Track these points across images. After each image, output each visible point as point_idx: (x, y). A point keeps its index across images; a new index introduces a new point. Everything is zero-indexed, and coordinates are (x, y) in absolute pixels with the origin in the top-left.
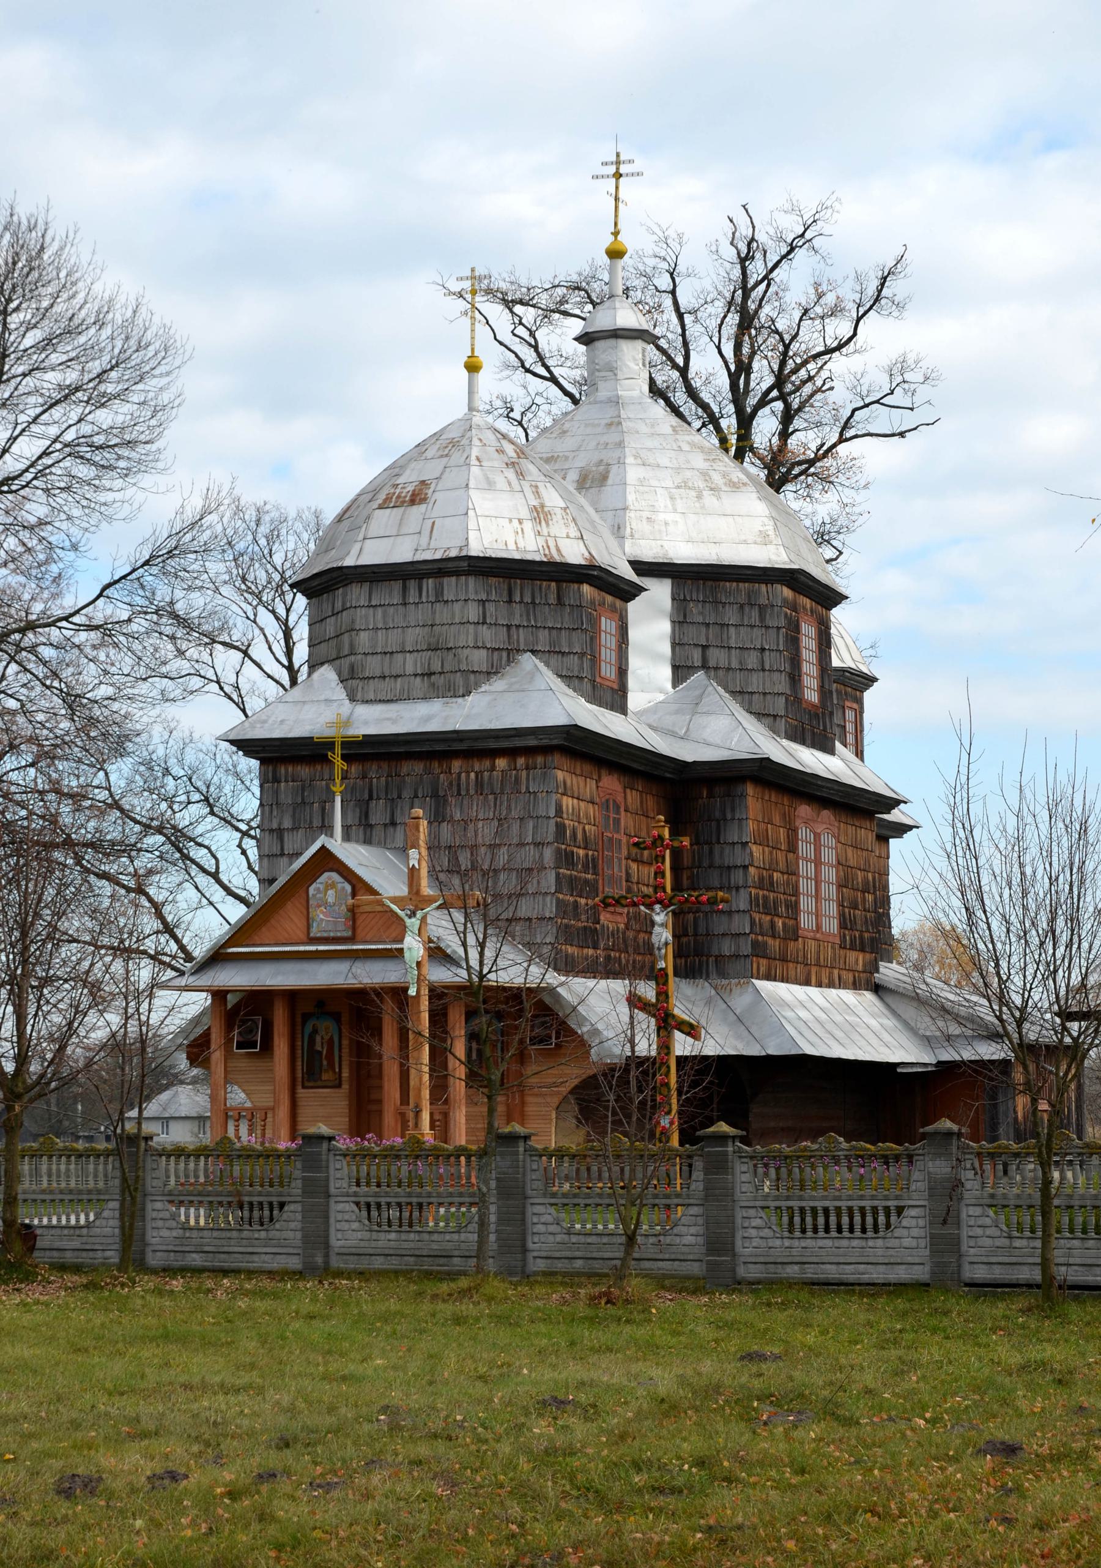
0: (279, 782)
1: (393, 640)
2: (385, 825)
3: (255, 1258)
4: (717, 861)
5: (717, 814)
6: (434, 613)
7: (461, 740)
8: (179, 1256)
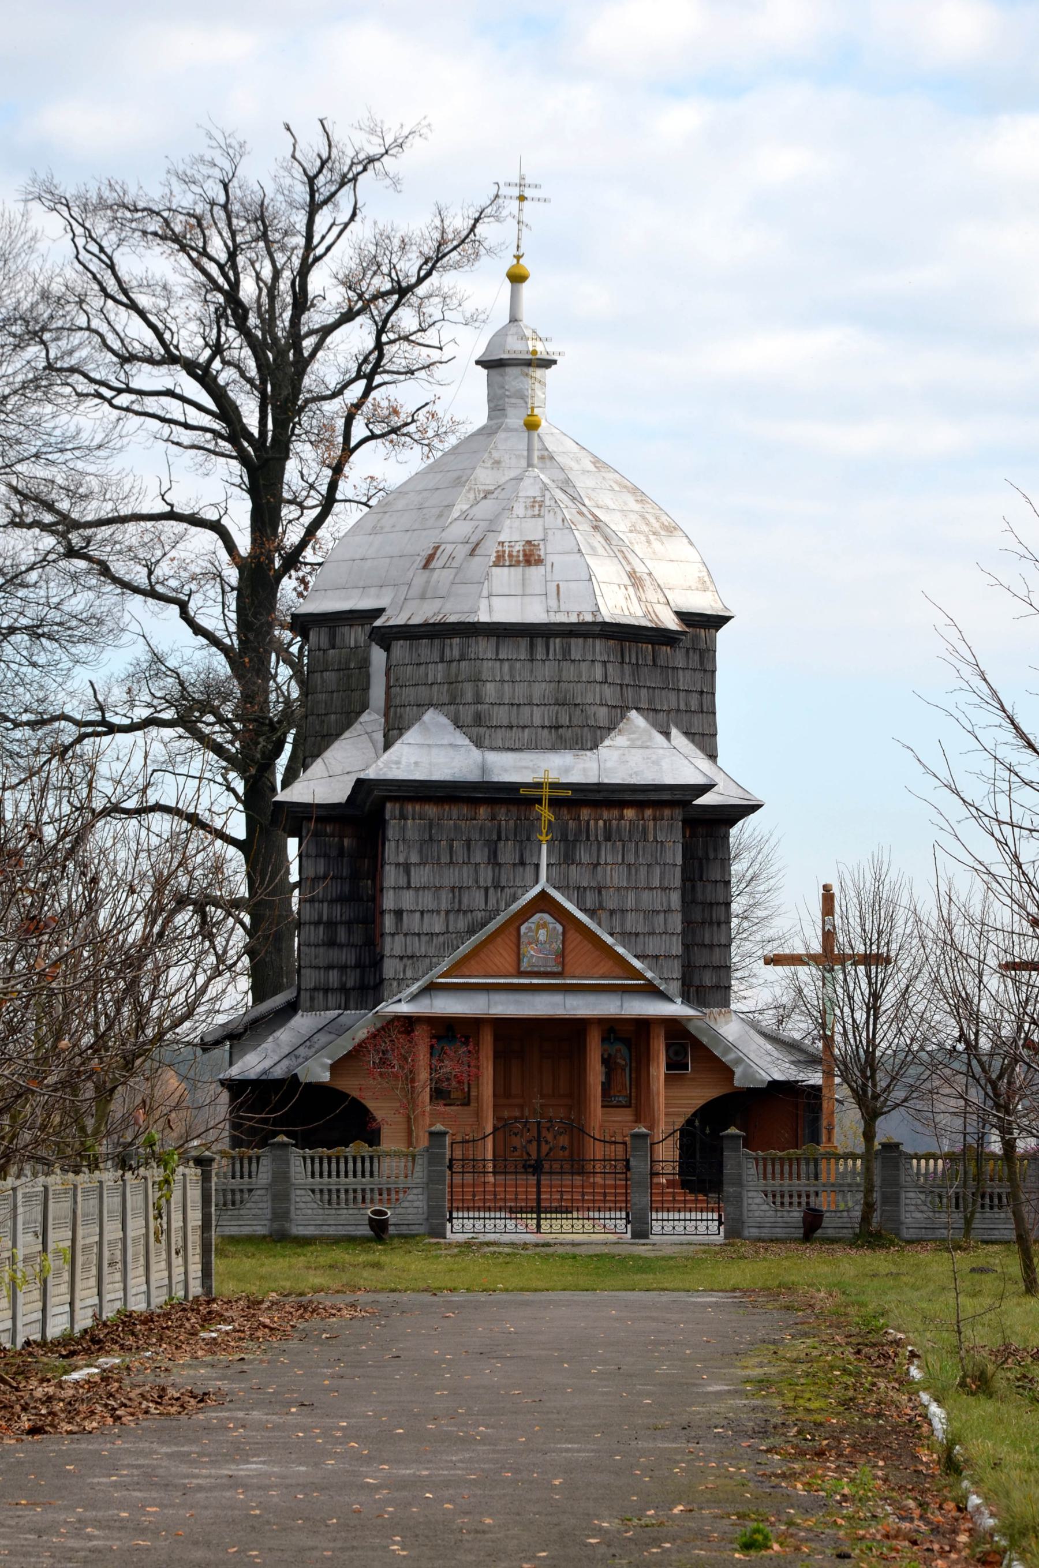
0: (406, 819)
1: (520, 692)
2: (514, 865)
3: (996, 1232)
4: (700, 897)
5: (700, 853)
6: (560, 671)
7: (599, 791)
8: (929, 1232)
